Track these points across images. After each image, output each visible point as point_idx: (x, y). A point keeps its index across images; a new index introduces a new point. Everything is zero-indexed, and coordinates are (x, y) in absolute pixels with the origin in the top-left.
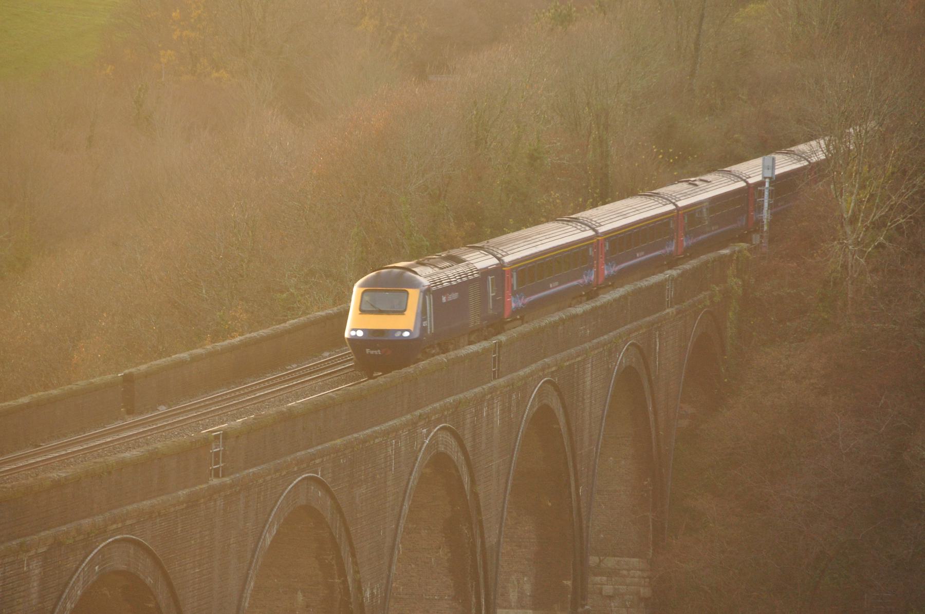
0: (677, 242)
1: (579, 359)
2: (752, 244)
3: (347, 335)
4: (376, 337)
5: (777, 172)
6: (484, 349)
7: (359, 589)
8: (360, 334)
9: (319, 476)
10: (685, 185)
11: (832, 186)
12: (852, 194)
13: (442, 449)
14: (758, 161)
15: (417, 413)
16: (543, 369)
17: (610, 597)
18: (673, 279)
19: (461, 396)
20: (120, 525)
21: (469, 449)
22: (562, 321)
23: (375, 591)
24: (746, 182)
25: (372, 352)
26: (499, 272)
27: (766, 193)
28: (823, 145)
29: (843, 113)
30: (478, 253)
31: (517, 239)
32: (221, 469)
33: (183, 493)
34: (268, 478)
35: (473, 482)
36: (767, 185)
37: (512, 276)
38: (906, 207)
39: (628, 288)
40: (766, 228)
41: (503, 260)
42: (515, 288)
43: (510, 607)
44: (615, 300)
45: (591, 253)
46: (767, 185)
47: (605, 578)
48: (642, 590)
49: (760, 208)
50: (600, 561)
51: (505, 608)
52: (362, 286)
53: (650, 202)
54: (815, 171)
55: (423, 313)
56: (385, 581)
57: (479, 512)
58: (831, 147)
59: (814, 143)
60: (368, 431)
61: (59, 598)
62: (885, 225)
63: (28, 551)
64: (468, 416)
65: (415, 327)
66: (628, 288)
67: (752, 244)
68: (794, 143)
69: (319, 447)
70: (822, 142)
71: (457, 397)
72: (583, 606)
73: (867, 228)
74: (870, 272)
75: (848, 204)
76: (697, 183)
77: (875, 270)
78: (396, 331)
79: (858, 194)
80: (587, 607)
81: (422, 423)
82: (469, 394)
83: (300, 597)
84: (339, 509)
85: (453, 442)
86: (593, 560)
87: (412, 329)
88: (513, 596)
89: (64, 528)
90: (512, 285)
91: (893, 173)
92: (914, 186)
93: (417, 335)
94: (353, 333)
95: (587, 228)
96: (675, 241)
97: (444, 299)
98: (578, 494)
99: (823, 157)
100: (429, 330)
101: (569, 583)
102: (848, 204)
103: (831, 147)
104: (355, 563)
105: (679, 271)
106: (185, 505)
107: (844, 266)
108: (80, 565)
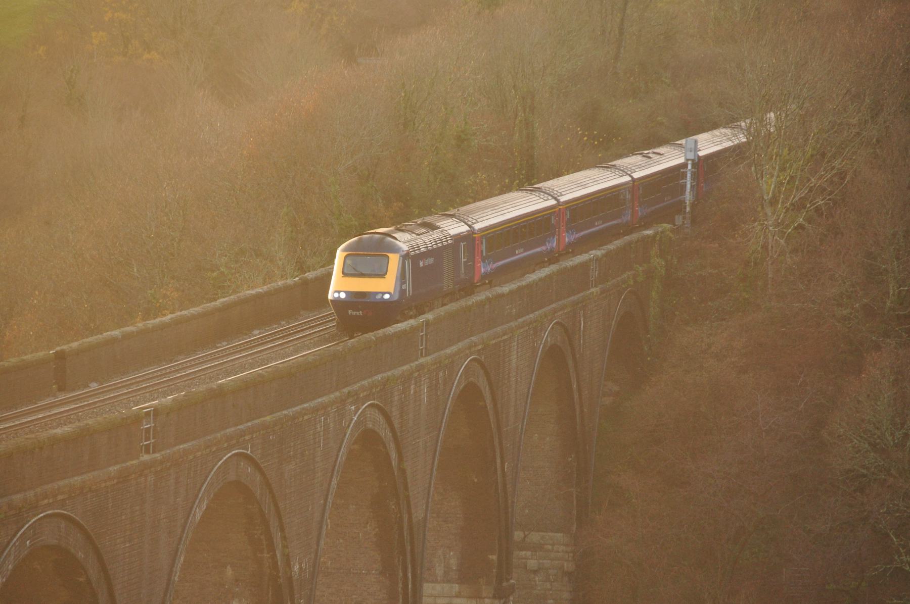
0: (559, 240)
4: (358, 299)
5: (701, 154)
6: (412, 327)
7: (288, 564)
11: (753, 168)
12: (772, 176)
15: (346, 390)
16: (470, 348)
17: (535, 572)
18: (597, 260)
19: (389, 373)
23: (303, 565)
25: (354, 313)
27: (689, 175)
30: (451, 220)
33: (113, 469)
35: (401, 458)
36: (690, 167)
38: (825, 189)
40: (688, 209)
43: (436, 581)
44: (541, 280)
46: (690, 167)
49: (683, 191)
50: (525, 536)
51: (432, 582)
52: (344, 250)
53: (608, 173)
54: (736, 152)
55: (402, 277)
56: (313, 556)
57: (406, 488)
62: (805, 207)
69: (249, 424)
71: (385, 375)
72: (508, 580)
73: (787, 210)
75: (768, 186)
77: (795, 251)
78: (377, 293)
79: (778, 176)
80: (512, 581)
81: (350, 400)
82: (397, 372)
83: (229, 571)
85: (381, 419)
86: (518, 535)
87: (392, 291)
88: (439, 571)
91: (812, 156)
92: (833, 168)
93: (396, 297)
101: (494, 557)
102: (768, 186)
104: (284, 538)
107: (765, 247)
108: (12, 539)
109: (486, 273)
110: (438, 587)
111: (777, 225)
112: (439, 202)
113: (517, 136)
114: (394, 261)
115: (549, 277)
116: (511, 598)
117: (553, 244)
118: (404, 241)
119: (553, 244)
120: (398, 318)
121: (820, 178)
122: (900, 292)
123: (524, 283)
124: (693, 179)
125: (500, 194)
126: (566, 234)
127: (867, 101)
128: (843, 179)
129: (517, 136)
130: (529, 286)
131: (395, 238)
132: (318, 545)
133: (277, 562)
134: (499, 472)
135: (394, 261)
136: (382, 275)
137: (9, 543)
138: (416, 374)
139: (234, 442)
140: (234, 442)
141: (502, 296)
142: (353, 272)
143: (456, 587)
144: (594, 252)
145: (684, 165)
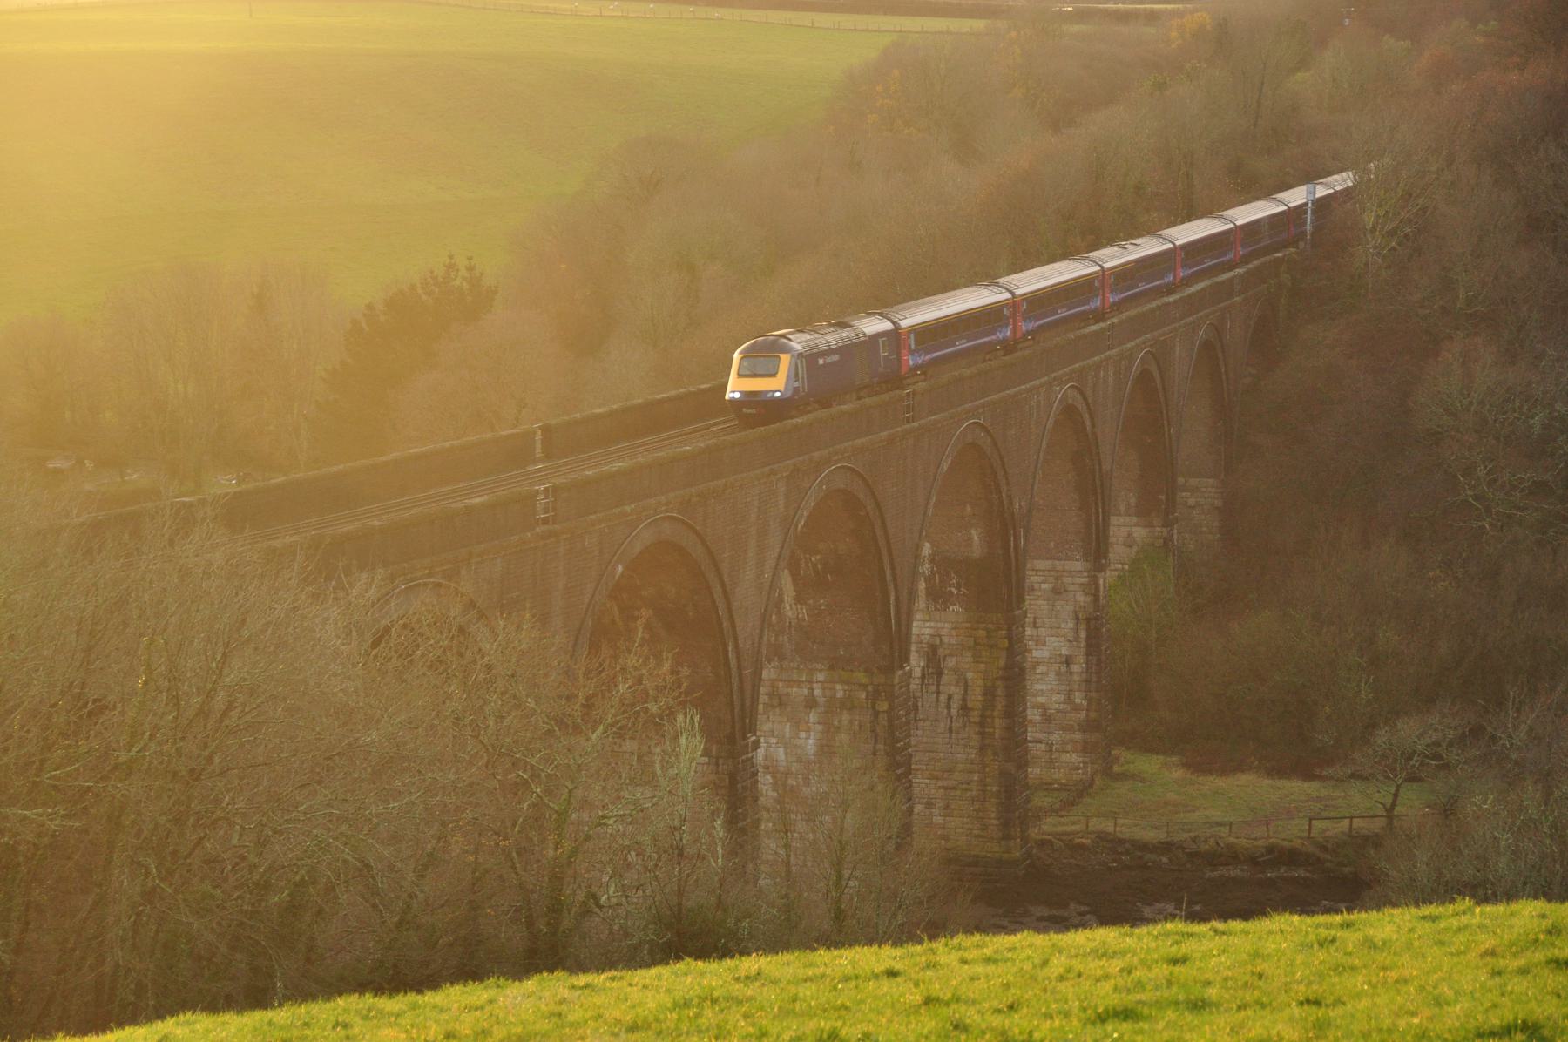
0: (1235, 253)
1: (1171, 335)
2: (1298, 248)
3: (727, 397)
4: (750, 398)
5: (1317, 196)
6: (1101, 329)
7: (1011, 503)
8: (737, 395)
9: (981, 422)
10: (1116, 248)
11: (1358, 206)
12: (1372, 211)
13: (1070, 401)
14: (1304, 188)
15: (1053, 375)
16: (1144, 343)
17: (1193, 507)
18: (1241, 275)
19: (1085, 363)
20: (840, 457)
21: (1090, 401)
22: (1159, 307)
23: (1022, 504)
24: (1173, 243)
26: (895, 335)
27: (1309, 212)
28: (1351, 176)
29: (1366, 151)
31: (923, 304)
32: (551, 518)
33: (884, 434)
34: (945, 423)
35: (1093, 426)
36: (1310, 205)
37: (909, 338)
38: (1412, 220)
39: (1206, 283)
40: (1308, 237)
41: (899, 325)
42: (913, 347)
43: (1120, 515)
44: (1198, 291)
45: (1096, 284)
46: (1310, 205)
47: (1189, 494)
48: (1216, 501)
49: (1305, 223)
50: (1186, 482)
51: (1117, 515)
52: (741, 353)
53: (1270, 204)
54: (1347, 193)
55: (794, 375)
56: (1029, 496)
57: (1097, 447)
58: (1357, 177)
59: (1344, 174)
60: (1015, 390)
61: (799, 507)
62: (1396, 233)
63: (776, 474)
64: (1090, 377)
65: (786, 388)
66: (1206, 283)
67: (1298, 248)
68: (1330, 174)
69: (982, 401)
70: (1350, 173)
71: (1081, 364)
72: (1173, 514)
73: (1383, 236)
74: (1386, 268)
75: (1369, 219)
76: (1126, 246)
77: (1389, 267)
78: (767, 392)
79: (1377, 211)
80: (1176, 514)
81: (1056, 383)
82: (1090, 361)
83: (969, 508)
84: (995, 444)
85: (1079, 397)
86: (1181, 480)
87: (782, 389)
88: (1122, 508)
89: (801, 459)
90: (910, 345)
91: (1402, 195)
92: (1417, 205)
93: (789, 394)
94: (732, 395)
95: (1004, 291)
96: (1233, 251)
97: (821, 362)
98: (1169, 434)
99: (1351, 184)
100: (801, 390)
101: (1162, 497)
102: (1369, 219)
103: (1357, 177)
104: (1008, 484)
105: (1244, 270)
106: (427, 571)
107: (1366, 264)
108: (812, 484)
109: (1114, 302)
110: (1122, 520)
111: (1375, 248)
112: (1121, 235)
113: (1180, 185)
114: (785, 360)
115: (1203, 289)
116: (1175, 526)
117: (1230, 256)
118: (799, 342)
119: (1230, 256)
120: (794, 413)
121: (1408, 212)
122: (1467, 296)
123: (1185, 294)
124: (1312, 213)
125: (1168, 228)
126: (1240, 249)
127: (1444, 154)
128: (1425, 212)
129: (1180, 185)
130: (1190, 296)
131: (790, 340)
132: (1033, 489)
133: (1002, 502)
134: (1166, 436)
135: (785, 360)
136: (773, 375)
137: (810, 488)
138: (1104, 363)
139: (971, 414)
140: (971, 414)
141: (1168, 304)
142: (748, 373)
143: (1135, 519)
144: (1237, 270)
145: (1306, 204)
